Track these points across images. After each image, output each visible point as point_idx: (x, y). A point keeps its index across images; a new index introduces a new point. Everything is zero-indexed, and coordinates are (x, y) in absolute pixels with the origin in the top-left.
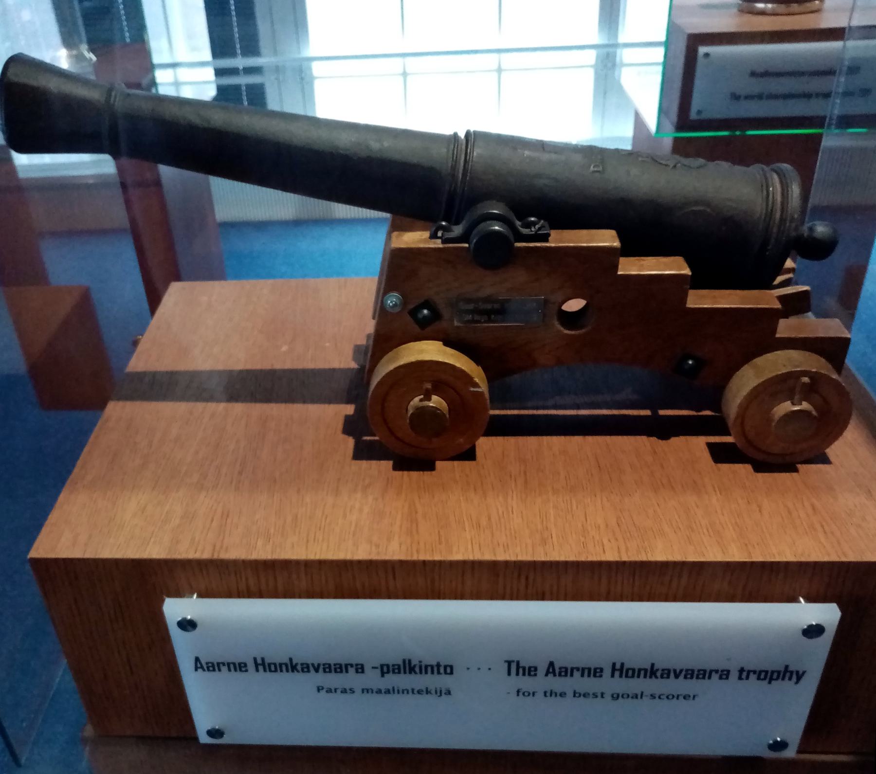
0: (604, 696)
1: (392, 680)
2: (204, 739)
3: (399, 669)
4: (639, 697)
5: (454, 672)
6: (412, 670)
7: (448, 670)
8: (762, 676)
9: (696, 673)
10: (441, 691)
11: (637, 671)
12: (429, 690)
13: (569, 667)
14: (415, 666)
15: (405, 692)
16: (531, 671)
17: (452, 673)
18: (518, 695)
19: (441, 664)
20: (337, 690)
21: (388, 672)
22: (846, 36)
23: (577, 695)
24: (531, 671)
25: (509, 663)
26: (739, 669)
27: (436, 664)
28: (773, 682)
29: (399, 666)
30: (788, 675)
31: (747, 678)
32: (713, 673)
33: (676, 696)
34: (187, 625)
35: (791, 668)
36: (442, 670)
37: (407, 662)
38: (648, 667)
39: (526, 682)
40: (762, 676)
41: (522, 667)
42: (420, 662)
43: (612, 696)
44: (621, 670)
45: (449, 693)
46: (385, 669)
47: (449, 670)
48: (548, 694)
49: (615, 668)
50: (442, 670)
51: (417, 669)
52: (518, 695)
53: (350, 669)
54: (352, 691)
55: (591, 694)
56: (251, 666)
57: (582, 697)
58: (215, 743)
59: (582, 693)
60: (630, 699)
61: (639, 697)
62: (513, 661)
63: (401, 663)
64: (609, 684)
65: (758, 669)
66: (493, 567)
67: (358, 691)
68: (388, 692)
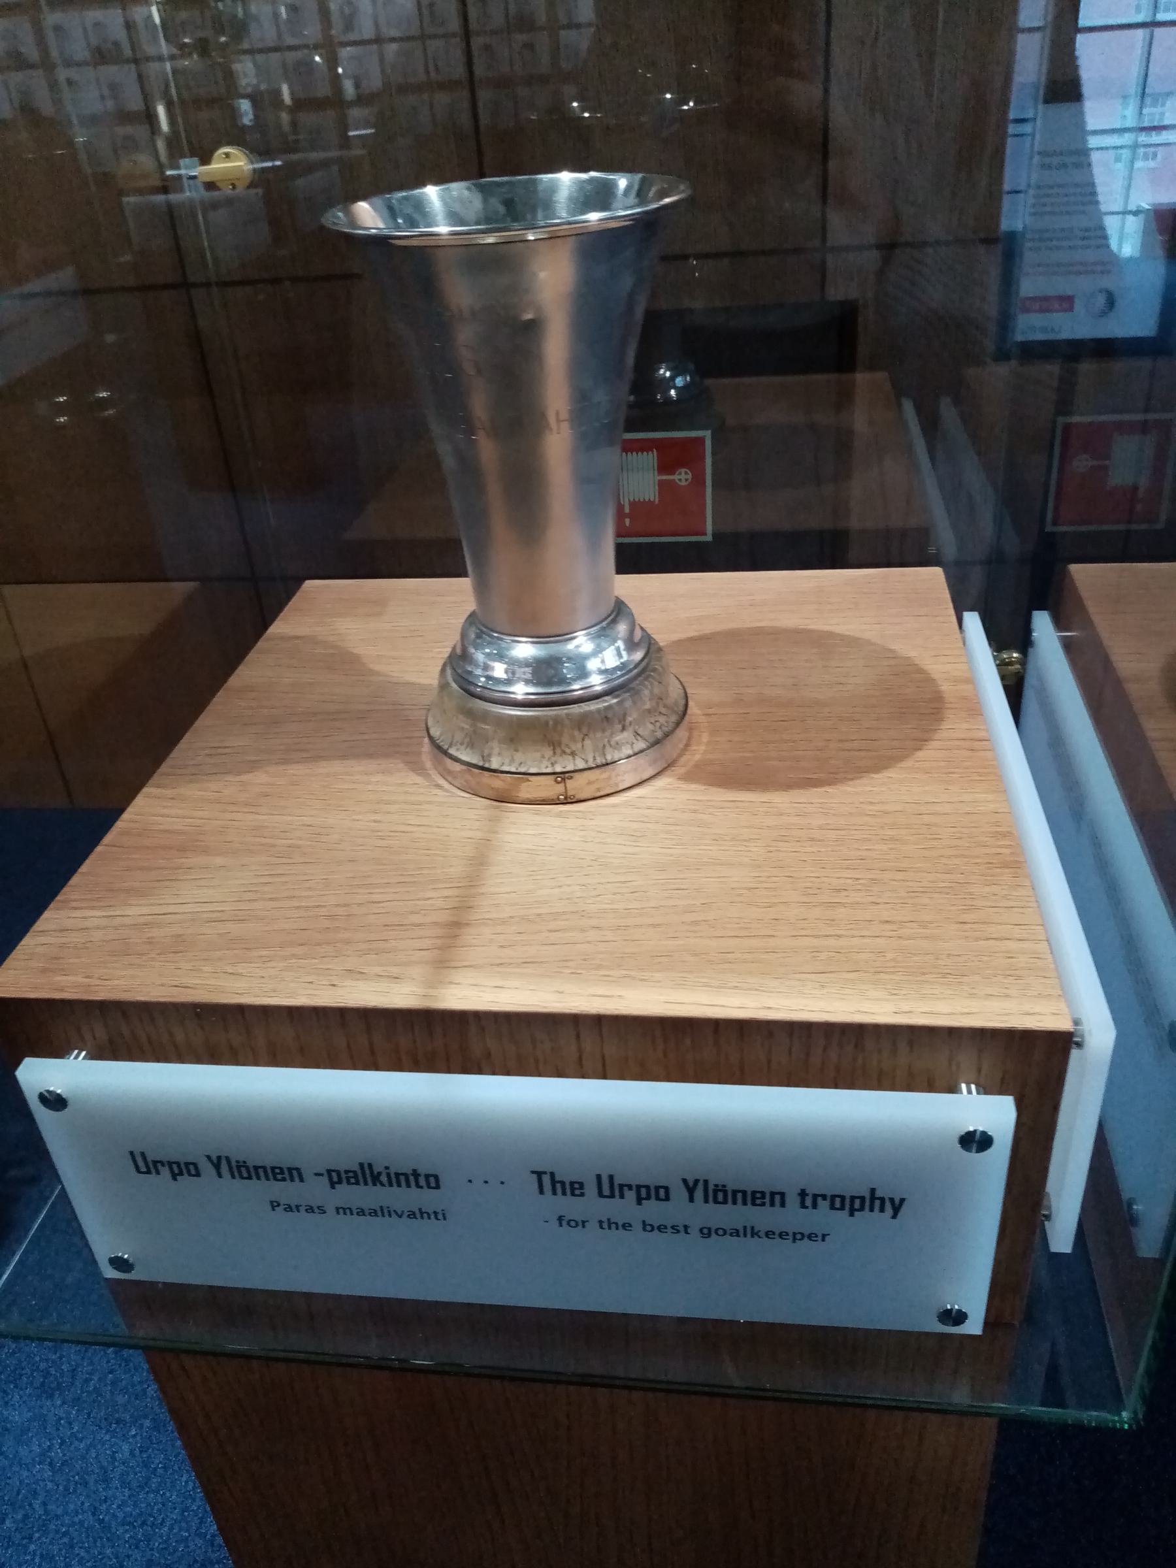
0: (689, 1231)
3: (356, 1177)
4: (741, 1234)
5: (671, 1196)
6: (376, 1179)
9: (767, 1200)
11: (749, 1194)
12: (756, 1231)
14: (379, 1174)
16: (575, 1188)
18: (561, 1225)
20: (300, 1208)
21: (648, 1198)
23: (649, 1228)
25: (539, 1174)
34: (55, 1102)
35: (878, 1194)
36: (422, 1182)
37: (366, 1166)
40: (838, 1205)
41: (878, 1198)
42: (387, 1168)
43: (701, 1230)
44: (610, 1187)
46: (335, 1178)
47: (433, 1181)
48: (605, 1225)
49: (554, 1180)
50: (422, 1182)
51: (384, 1178)
52: (561, 1225)
53: (627, 1193)
54: (322, 1210)
56: (591, 1189)
57: (656, 1231)
58: (123, 1278)
59: (656, 1225)
60: (728, 1236)
61: (741, 1234)
62: (545, 1173)
63: (357, 1168)
65: (829, 1194)
67: (331, 1210)
68: (374, 1213)
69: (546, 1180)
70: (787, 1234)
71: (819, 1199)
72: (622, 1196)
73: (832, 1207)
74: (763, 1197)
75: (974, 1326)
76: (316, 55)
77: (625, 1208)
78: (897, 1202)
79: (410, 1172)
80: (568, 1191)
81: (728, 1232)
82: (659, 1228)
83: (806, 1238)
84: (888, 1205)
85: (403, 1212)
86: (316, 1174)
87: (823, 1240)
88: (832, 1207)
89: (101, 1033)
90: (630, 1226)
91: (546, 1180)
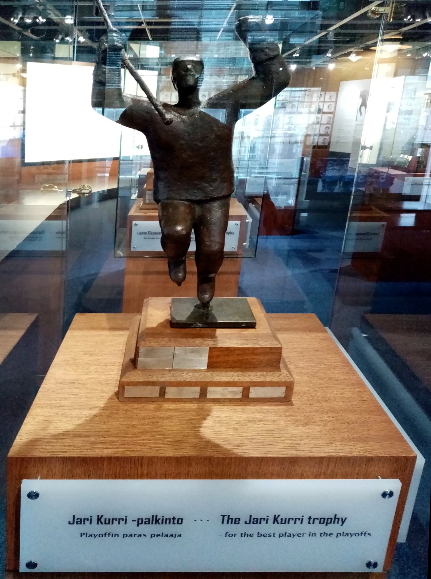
1: (144, 529)
2: (23, 569)
6: (157, 521)
7: (180, 522)
8: (322, 521)
9: (144, 521)
10: (175, 535)
13: (259, 518)
15: (117, 536)
16: (237, 521)
17: (181, 523)
19: (175, 518)
22: (124, 307)
24: (237, 521)
25: (224, 516)
26: (309, 517)
27: (173, 518)
28: (328, 525)
29: (149, 519)
30: (336, 520)
31: (313, 523)
32: (316, 520)
33: (328, 535)
38: (333, 517)
39: (231, 528)
40: (322, 521)
41: (230, 519)
42: (163, 517)
45: (180, 536)
46: (140, 522)
47: (180, 521)
54: (145, 536)
55: (268, 534)
62: (226, 515)
64: (271, 528)
65: (319, 517)
66: (321, 460)
67: (318, 535)
69: (226, 518)
70: (301, 534)
71: (121, 520)
72: (112, 523)
73: (320, 523)
74: (145, 522)
75: (379, 570)
76: (308, 214)
77: (318, 528)
78: (344, 519)
79: (171, 518)
80: (233, 522)
81: (128, 535)
82: (157, 536)
83: (262, 536)
84: (279, 522)
85: (97, 535)
86: (133, 521)
87: (303, 536)
88: (320, 523)
89: (45, 471)
90: (253, 535)
91: (226, 518)
